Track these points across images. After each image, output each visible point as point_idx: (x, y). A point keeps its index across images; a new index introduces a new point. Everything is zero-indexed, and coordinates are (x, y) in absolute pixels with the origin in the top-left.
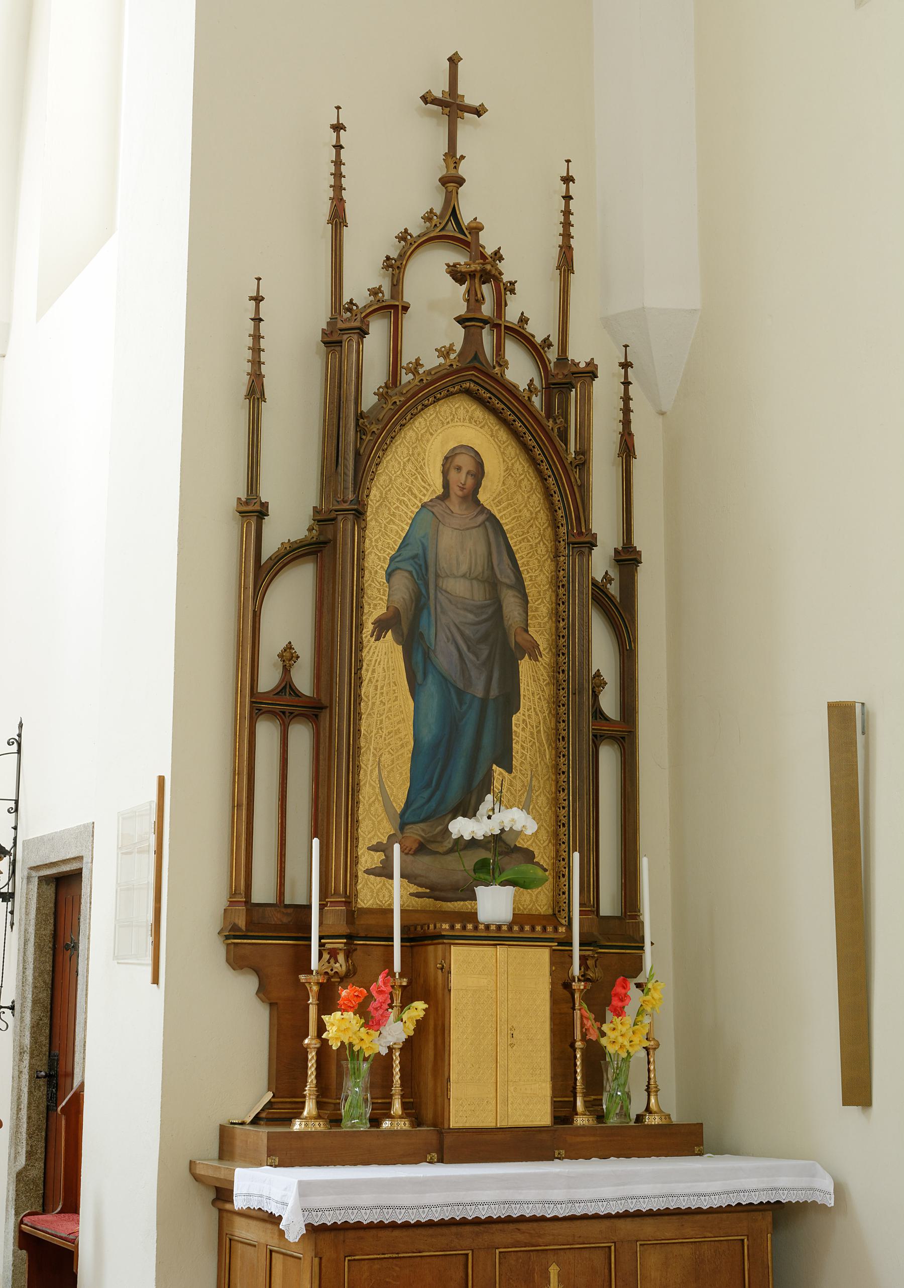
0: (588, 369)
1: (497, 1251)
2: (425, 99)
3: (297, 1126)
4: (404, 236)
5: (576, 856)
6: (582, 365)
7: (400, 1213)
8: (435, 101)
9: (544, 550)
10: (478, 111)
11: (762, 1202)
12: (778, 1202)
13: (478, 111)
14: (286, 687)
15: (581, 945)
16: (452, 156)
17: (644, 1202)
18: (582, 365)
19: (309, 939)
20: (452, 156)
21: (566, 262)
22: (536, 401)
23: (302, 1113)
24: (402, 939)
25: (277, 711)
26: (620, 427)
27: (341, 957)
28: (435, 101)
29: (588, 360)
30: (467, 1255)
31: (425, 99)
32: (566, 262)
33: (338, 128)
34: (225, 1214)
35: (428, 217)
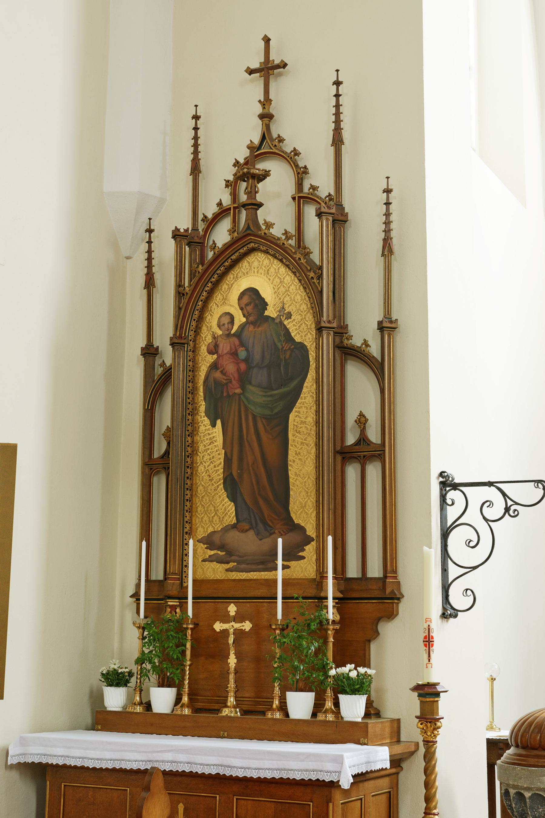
0: (185, 234)
1: (311, 804)
2: (285, 65)
3: (226, 712)
4: (296, 153)
5: (330, 538)
6: (182, 231)
7: (135, 764)
8: (278, 67)
9: (311, 338)
10: (251, 72)
11: (318, 779)
12: (332, 781)
13: (251, 72)
14: (363, 440)
15: (193, 598)
16: (266, 102)
17: (314, 774)
18: (182, 231)
19: (146, 599)
20: (266, 102)
21: (337, 141)
22: (210, 255)
23: (272, 706)
24: (282, 597)
25: (376, 455)
26: (146, 270)
27: (178, 610)
28: (278, 67)
29: (186, 228)
30: (65, 785)
31: (285, 65)
32: (337, 141)
33: (338, 83)
34: (395, 776)
35: (281, 140)
